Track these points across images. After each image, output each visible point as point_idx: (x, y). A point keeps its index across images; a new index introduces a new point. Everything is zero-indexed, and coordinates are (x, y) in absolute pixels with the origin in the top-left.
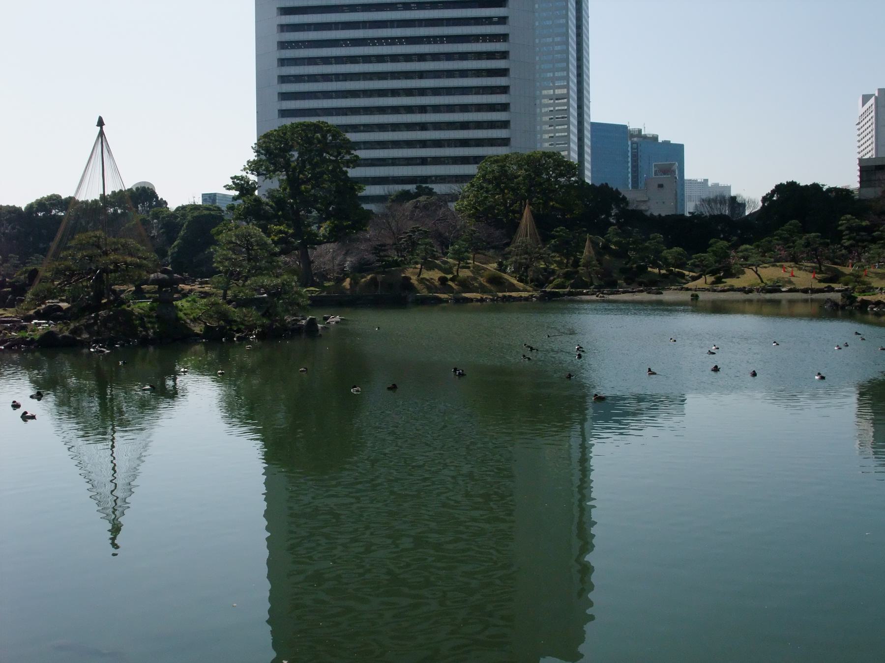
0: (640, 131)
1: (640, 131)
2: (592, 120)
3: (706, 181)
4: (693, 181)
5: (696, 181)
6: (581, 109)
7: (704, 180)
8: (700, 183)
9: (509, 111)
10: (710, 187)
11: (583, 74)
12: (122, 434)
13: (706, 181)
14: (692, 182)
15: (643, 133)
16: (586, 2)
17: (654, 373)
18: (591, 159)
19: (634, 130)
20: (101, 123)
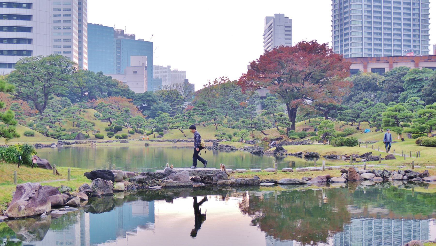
0: (123, 31)
1: (123, 31)
2: (89, 22)
3: (169, 67)
4: (160, 66)
5: (162, 66)
6: (81, 49)
7: (168, 66)
8: (165, 68)
9: (32, 32)
10: (172, 71)
11: (83, 8)
12: (9, 198)
13: (169, 67)
14: (159, 67)
15: (125, 33)
16: (85, 12)
17: (58, 174)
18: (88, 46)
19: (118, 31)
20: (194, 234)
